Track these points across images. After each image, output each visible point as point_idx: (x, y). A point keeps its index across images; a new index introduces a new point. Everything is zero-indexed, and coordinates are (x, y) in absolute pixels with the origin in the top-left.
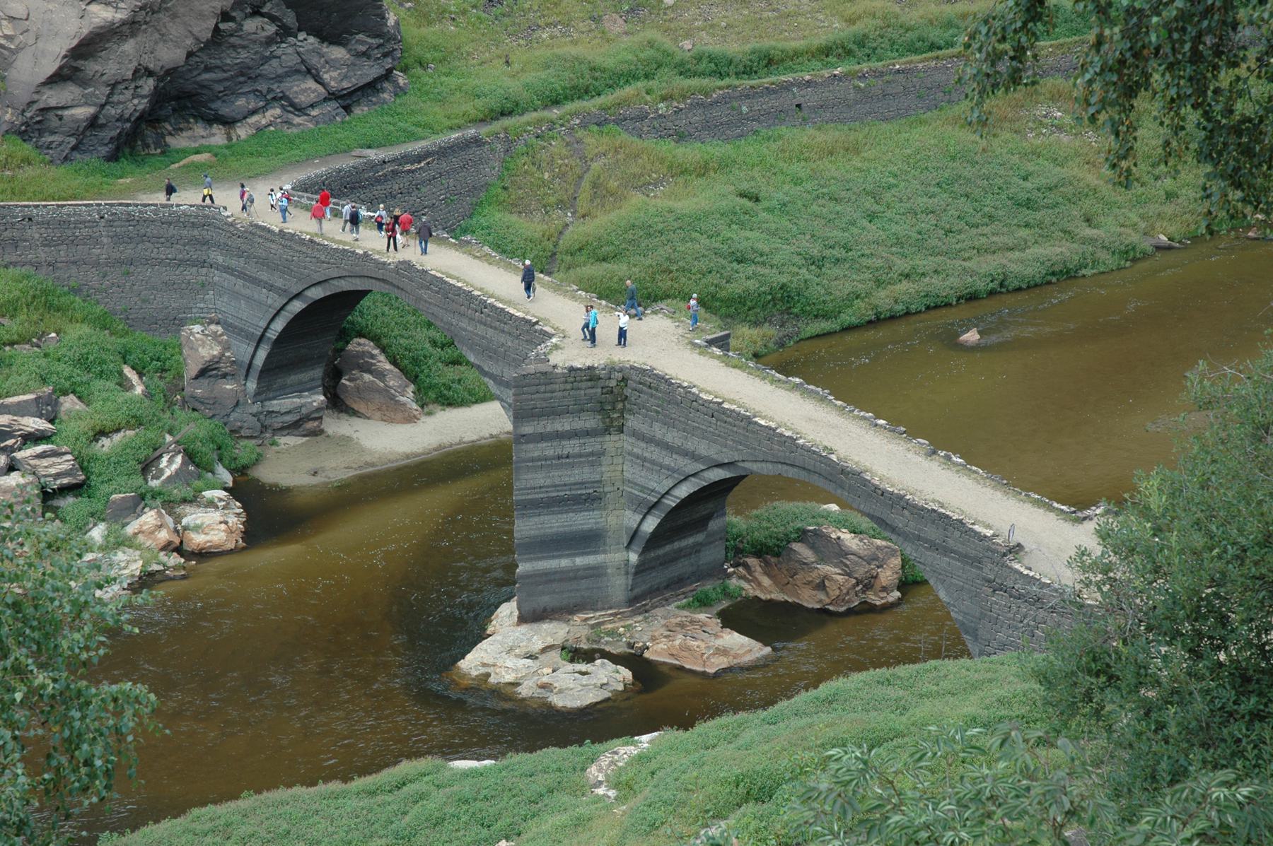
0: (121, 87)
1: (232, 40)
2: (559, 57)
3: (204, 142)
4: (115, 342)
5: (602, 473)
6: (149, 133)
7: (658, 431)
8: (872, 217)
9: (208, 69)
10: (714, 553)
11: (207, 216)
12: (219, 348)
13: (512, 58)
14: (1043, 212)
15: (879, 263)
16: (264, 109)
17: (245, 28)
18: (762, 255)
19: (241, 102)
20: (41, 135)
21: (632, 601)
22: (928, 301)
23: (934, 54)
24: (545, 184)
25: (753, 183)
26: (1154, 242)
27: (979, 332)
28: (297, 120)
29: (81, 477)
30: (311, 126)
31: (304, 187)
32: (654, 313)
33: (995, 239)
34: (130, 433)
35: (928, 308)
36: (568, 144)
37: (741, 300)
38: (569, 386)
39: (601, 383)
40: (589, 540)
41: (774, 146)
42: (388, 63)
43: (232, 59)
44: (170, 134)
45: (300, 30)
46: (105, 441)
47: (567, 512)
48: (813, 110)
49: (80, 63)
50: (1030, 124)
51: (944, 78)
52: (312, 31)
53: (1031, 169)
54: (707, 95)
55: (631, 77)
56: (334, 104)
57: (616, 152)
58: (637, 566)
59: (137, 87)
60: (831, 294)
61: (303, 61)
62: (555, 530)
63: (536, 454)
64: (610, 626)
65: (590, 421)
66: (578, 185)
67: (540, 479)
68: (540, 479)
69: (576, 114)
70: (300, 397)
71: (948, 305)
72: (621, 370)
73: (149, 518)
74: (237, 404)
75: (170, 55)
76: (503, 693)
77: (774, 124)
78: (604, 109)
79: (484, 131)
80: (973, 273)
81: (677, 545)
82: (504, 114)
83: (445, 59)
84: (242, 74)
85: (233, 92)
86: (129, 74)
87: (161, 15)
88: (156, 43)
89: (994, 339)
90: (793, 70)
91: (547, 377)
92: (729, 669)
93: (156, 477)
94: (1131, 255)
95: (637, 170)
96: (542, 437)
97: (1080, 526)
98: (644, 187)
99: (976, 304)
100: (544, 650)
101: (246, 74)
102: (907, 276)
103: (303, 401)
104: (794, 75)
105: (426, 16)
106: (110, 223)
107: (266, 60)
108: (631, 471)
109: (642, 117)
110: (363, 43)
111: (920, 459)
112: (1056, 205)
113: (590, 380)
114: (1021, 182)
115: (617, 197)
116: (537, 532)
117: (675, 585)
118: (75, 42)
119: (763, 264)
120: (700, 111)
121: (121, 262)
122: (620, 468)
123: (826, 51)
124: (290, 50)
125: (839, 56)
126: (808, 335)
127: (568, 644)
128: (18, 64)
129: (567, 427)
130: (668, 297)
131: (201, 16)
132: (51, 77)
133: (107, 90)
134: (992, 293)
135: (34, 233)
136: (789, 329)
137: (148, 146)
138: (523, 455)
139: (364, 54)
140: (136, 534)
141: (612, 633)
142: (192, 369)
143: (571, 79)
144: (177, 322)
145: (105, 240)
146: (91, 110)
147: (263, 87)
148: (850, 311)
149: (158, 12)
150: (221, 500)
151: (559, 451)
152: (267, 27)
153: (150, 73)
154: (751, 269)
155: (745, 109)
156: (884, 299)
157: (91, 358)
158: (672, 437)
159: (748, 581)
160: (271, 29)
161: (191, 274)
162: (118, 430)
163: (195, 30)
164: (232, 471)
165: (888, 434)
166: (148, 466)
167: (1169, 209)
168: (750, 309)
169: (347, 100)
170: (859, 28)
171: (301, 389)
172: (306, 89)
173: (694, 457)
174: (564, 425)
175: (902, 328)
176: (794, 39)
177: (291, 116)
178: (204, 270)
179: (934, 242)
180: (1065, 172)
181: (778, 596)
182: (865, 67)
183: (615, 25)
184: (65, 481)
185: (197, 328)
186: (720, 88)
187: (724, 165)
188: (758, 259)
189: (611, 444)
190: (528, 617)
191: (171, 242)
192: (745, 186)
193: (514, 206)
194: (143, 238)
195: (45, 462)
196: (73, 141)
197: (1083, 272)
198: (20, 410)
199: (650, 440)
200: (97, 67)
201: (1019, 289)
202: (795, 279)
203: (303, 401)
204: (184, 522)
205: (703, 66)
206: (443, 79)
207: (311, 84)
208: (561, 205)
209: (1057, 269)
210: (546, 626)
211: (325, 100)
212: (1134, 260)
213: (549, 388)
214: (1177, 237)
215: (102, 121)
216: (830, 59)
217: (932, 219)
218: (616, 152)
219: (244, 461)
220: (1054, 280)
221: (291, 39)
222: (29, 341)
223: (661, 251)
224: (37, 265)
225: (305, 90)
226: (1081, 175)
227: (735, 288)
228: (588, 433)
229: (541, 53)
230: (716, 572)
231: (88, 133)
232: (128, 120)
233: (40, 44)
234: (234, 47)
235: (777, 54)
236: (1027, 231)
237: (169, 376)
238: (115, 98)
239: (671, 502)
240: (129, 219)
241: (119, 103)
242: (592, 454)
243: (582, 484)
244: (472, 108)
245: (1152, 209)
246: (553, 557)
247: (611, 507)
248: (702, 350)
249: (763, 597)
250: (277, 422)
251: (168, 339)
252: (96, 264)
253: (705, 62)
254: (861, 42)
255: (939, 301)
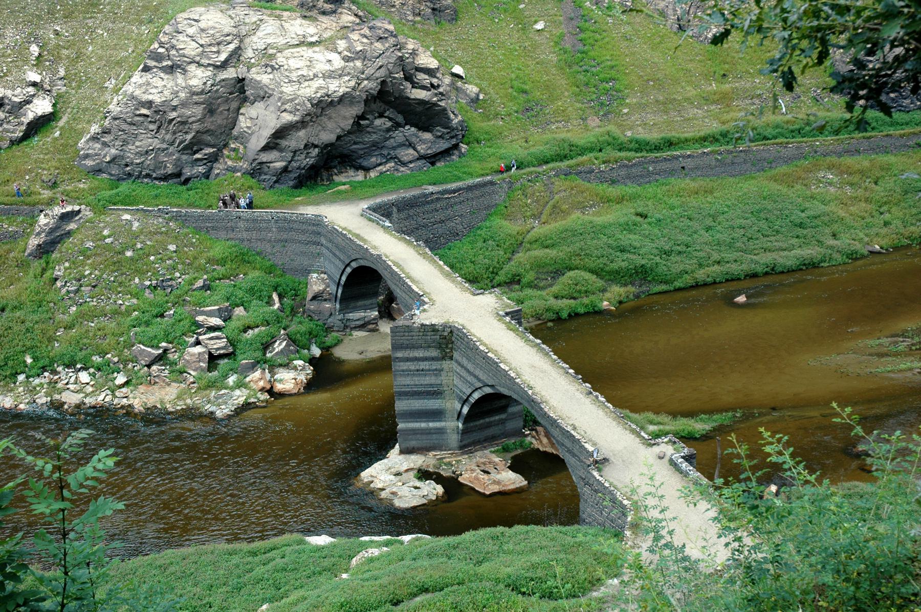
0: (298, 153)
1: (368, 129)
2: (554, 139)
3: (352, 179)
4: (272, 280)
5: (442, 381)
7: (465, 362)
8: (708, 229)
9: (355, 143)
10: (518, 423)
11: (319, 221)
12: (324, 286)
13: (530, 138)
14: (809, 230)
15: (702, 254)
16: (386, 163)
17: (375, 123)
18: (635, 248)
19: (373, 159)
20: (260, 175)
22: (728, 277)
23: (764, 142)
25: (646, 209)
26: (871, 249)
27: (747, 297)
28: (402, 169)
29: (231, 350)
30: (408, 172)
32: (490, 293)
33: (776, 244)
34: (263, 328)
35: (727, 280)
36: (545, 185)
37: (617, 272)
38: (421, 334)
39: (439, 333)
40: (437, 414)
41: (664, 188)
42: (454, 141)
43: (368, 138)
44: (336, 174)
45: (406, 124)
46: (250, 332)
47: (423, 399)
48: (691, 169)
49: (278, 141)
50: (814, 181)
51: (768, 155)
52: (416, 126)
53: (807, 206)
54: (630, 161)
55: (591, 150)
56: (424, 161)
57: (572, 189)
58: (462, 430)
59: (308, 153)
60: (670, 271)
61: (407, 140)
62: (417, 408)
63: (405, 368)
64: (448, 460)
65: (434, 353)
66: (545, 206)
67: (408, 381)
68: (408, 381)
69: (553, 169)
70: (365, 312)
71: (739, 279)
72: (450, 327)
73: (257, 374)
74: (331, 314)
75: (327, 137)
76: (373, 493)
77: (668, 177)
78: (571, 167)
80: (757, 263)
81: (487, 420)
83: (491, 139)
84: (374, 146)
85: (369, 154)
86: (302, 147)
87: (323, 118)
88: (320, 131)
89: (753, 300)
90: (682, 148)
92: (500, 493)
93: (271, 352)
94: (854, 257)
95: (582, 200)
96: (408, 360)
97: (650, 449)
98: (583, 208)
99: (756, 279)
100: (407, 471)
102: (719, 263)
103: (366, 314)
104: (681, 152)
105: (488, 117)
106: (276, 222)
107: (387, 139)
108: (457, 381)
109: (591, 171)
110: (439, 131)
111: (582, 396)
112: (817, 226)
113: (433, 331)
114: (800, 213)
115: (566, 213)
116: (407, 408)
117: (489, 441)
118: (274, 131)
119: (635, 253)
120: (626, 169)
122: (452, 378)
123: (704, 139)
124: (401, 134)
125: (711, 142)
126: (654, 292)
127: (422, 468)
128: (251, 141)
129: (421, 355)
130: (577, 269)
132: (263, 147)
133: (292, 154)
134: (766, 274)
135: (241, 224)
136: (644, 288)
137: (323, 180)
138: (397, 368)
139: (440, 137)
140: (250, 382)
142: (310, 296)
143: (556, 151)
145: (274, 229)
146: (284, 164)
147: (385, 152)
148: (680, 280)
149: (321, 116)
150: (300, 366)
151: (417, 367)
152: (387, 123)
153: (316, 146)
154: (626, 256)
155: (651, 169)
156: (701, 275)
157: (256, 289)
158: (470, 366)
159: (536, 439)
161: (313, 249)
162: (258, 327)
163: (342, 125)
164: (322, 349)
165: (571, 379)
166: (266, 346)
167: (884, 231)
168: (622, 277)
169: (432, 159)
170: (725, 128)
171: (365, 308)
172: (408, 154)
173: (479, 380)
174: (419, 353)
175: (708, 291)
176: (688, 132)
177: (399, 167)
178: (319, 247)
180: (827, 209)
181: (549, 449)
182: (722, 149)
183: (593, 122)
184: (222, 352)
185: (315, 275)
186: (637, 158)
187: (633, 198)
188: (633, 251)
189: (446, 366)
190: (404, 451)
191: (304, 232)
192: (640, 210)
193: (507, 217)
195: (212, 342)
196: (275, 178)
197: (822, 264)
199: (462, 366)
200: (287, 143)
201: (782, 272)
202: (650, 263)
203: (366, 314)
204: (275, 377)
205: (632, 145)
206: (487, 149)
207: (411, 151)
208: (534, 216)
209: (806, 262)
210: (413, 457)
211: (418, 159)
212: (856, 259)
213: (410, 334)
214: (885, 247)
215: (290, 169)
216: (706, 143)
217: (742, 231)
218: (572, 189)
219: (328, 344)
220: (804, 268)
221: (401, 129)
222: (229, 278)
223: (578, 244)
224: (243, 240)
225: (407, 154)
226: (835, 210)
227: (615, 266)
228: (433, 359)
229: (548, 136)
231: (283, 175)
232: (303, 169)
233: (261, 132)
234: (369, 133)
235: (674, 140)
236: (797, 240)
237: (298, 299)
238: (296, 158)
239: (472, 400)
240: (285, 219)
241: (298, 160)
242: (436, 370)
245: (874, 231)
246: (417, 422)
247: (448, 398)
248: (500, 318)
249: (541, 449)
250: (353, 324)
251: (302, 279)
253: (634, 143)
254: (724, 135)
255: (734, 277)
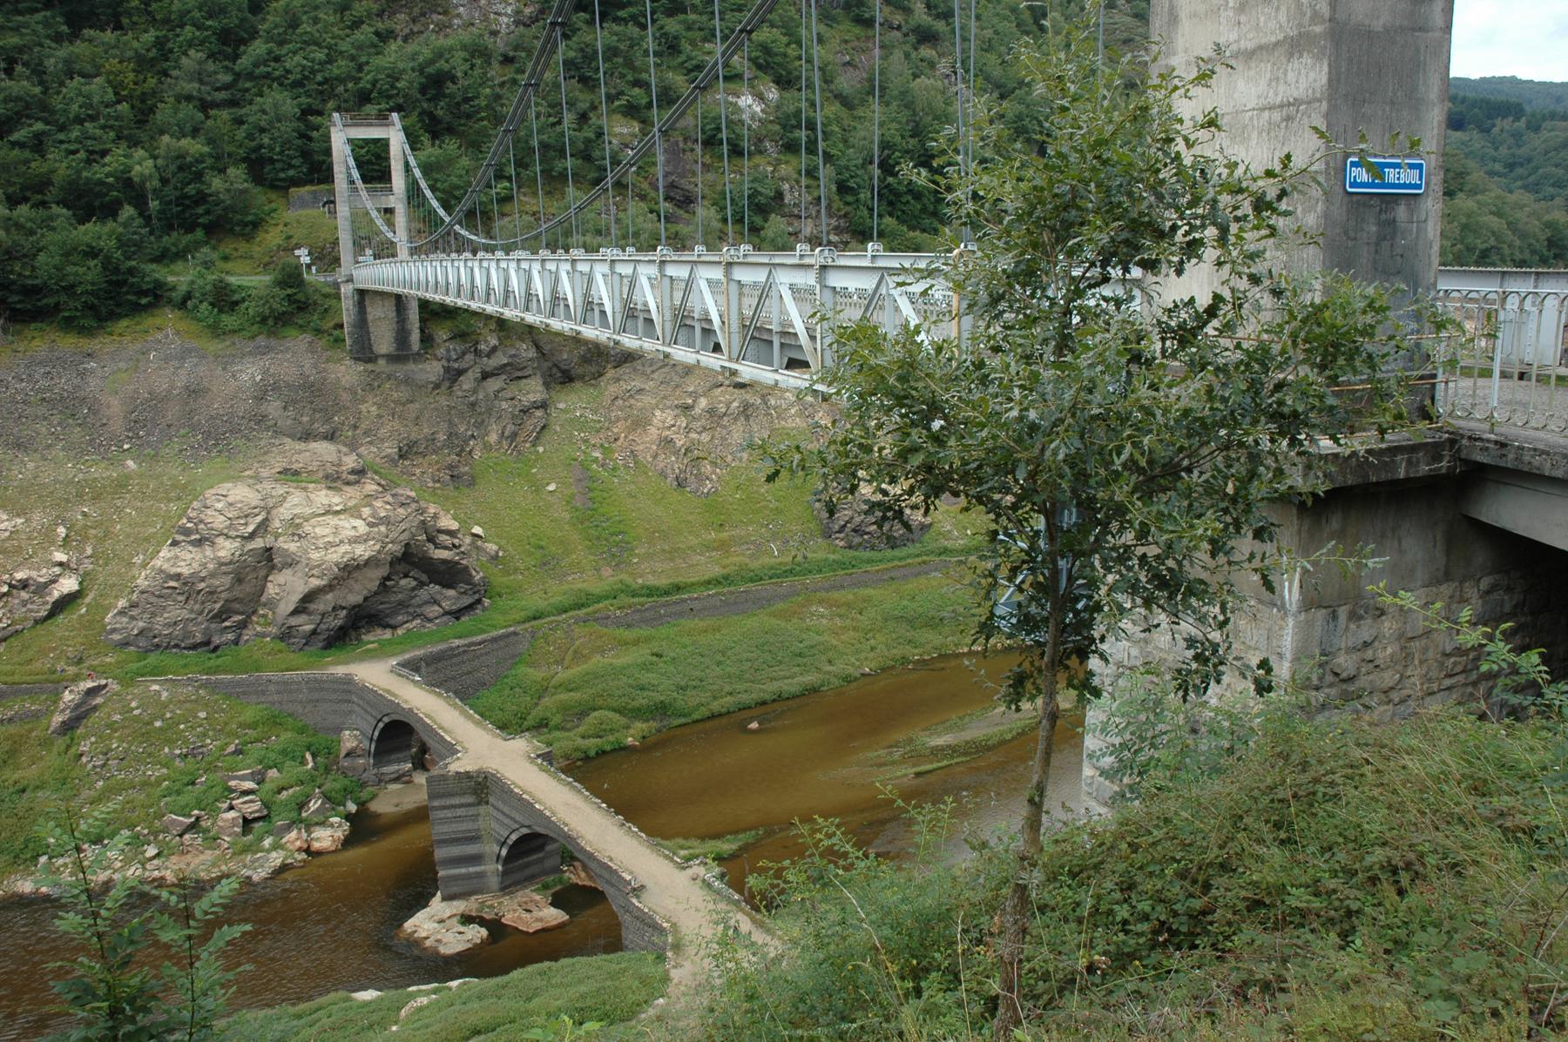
4: (305, 739)
6: (353, 634)
7: (500, 805)
8: (719, 663)
10: (556, 860)
19: (400, 618)
21: (502, 889)
24: (550, 653)
29: (265, 812)
31: (404, 665)
37: (639, 710)
40: (476, 859)
46: (285, 793)
48: (699, 611)
55: (607, 598)
65: (470, 799)
67: (445, 828)
68: (445, 828)
69: (572, 617)
75: (355, 598)
78: (588, 614)
79: (519, 629)
82: (535, 618)
85: (395, 613)
91: (444, 778)
94: (848, 680)
96: (445, 808)
100: (449, 917)
101: (402, 605)
109: (608, 618)
115: (586, 658)
121: (311, 701)
123: (709, 582)
131: (371, 580)
134: (774, 700)
135: (272, 688)
141: (492, 906)
144: (339, 730)
147: (411, 610)
153: (344, 608)
156: (716, 706)
158: (506, 810)
160: (414, 583)
161: (344, 707)
166: (302, 806)
167: (871, 655)
169: (457, 614)
170: (725, 571)
171: (399, 761)
174: (456, 801)
175: (724, 720)
179: (747, 676)
180: (821, 639)
181: (588, 883)
182: (725, 590)
183: (607, 572)
185: (347, 732)
187: (648, 640)
191: (335, 691)
193: (533, 665)
194: (322, 689)
198: (243, 778)
207: (437, 608)
208: (557, 663)
210: (455, 903)
212: (850, 682)
217: (749, 664)
227: (636, 704)
228: (469, 805)
229: (566, 587)
230: (557, 870)
235: (682, 585)
237: (332, 757)
239: (510, 842)
240: (316, 680)
243: (469, 831)
244: (519, 616)
245: (863, 656)
250: (387, 778)
251: (335, 737)
252: (301, 702)
254: (726, 578)
